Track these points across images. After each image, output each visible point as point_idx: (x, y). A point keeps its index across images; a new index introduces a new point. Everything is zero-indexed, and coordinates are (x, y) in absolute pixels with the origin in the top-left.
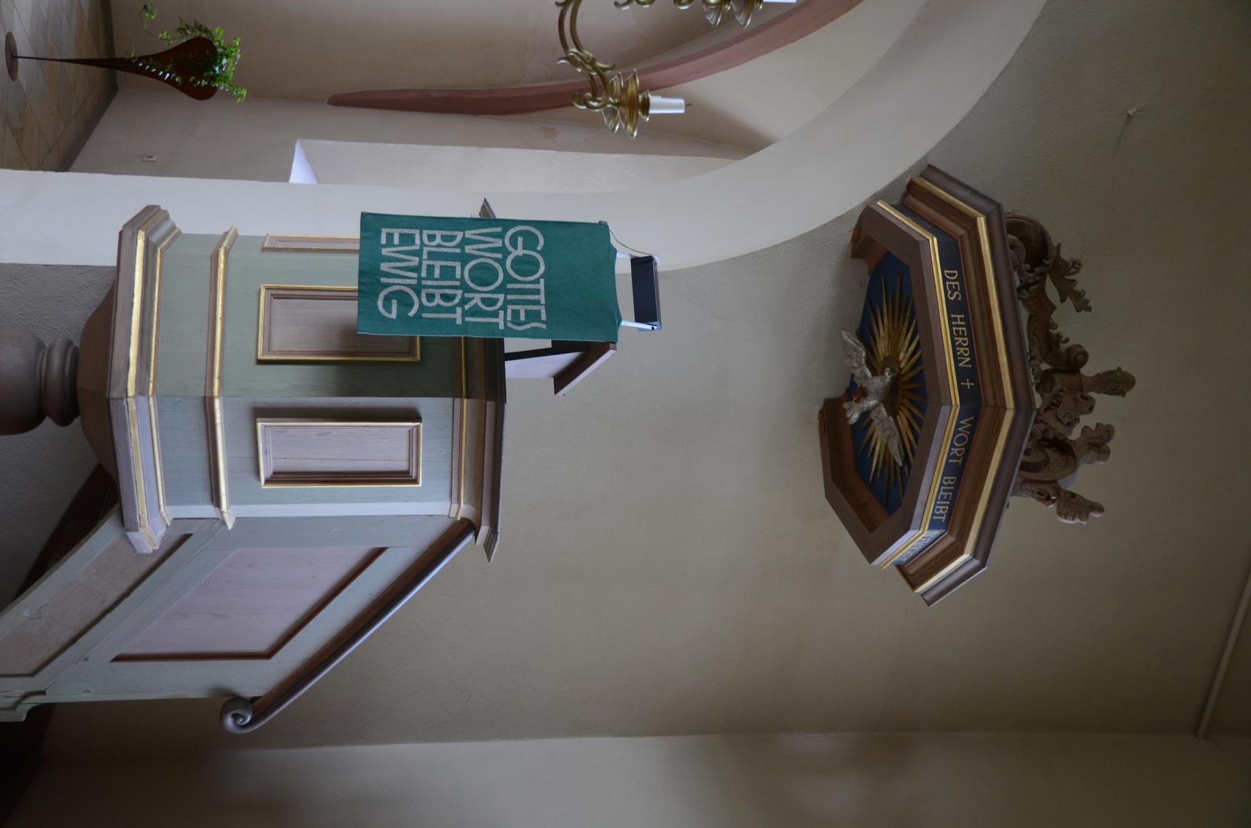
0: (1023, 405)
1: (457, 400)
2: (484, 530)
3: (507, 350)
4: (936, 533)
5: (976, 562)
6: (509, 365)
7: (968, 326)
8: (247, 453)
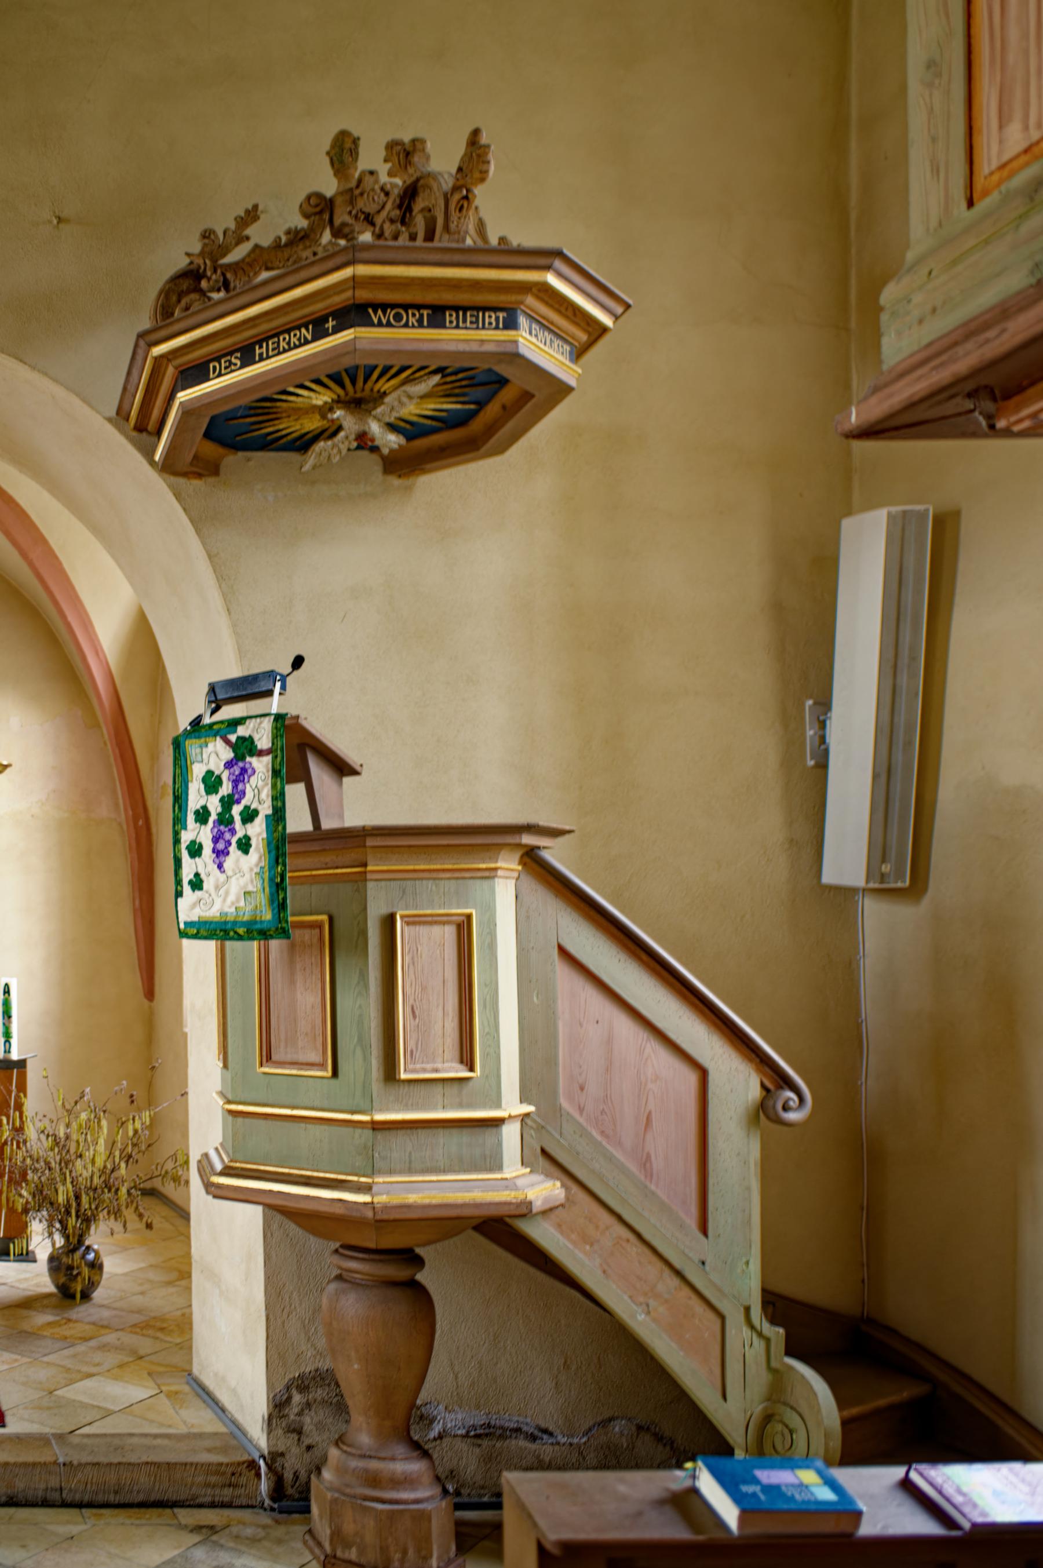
0: (354, 255)
1: (369, 876)
2: (528, 840)
3: (308, 826)
4: (522, 320)
5: (558, 264)
6: (326, 824)
7: (267, 339)
8: (438, 1089)
